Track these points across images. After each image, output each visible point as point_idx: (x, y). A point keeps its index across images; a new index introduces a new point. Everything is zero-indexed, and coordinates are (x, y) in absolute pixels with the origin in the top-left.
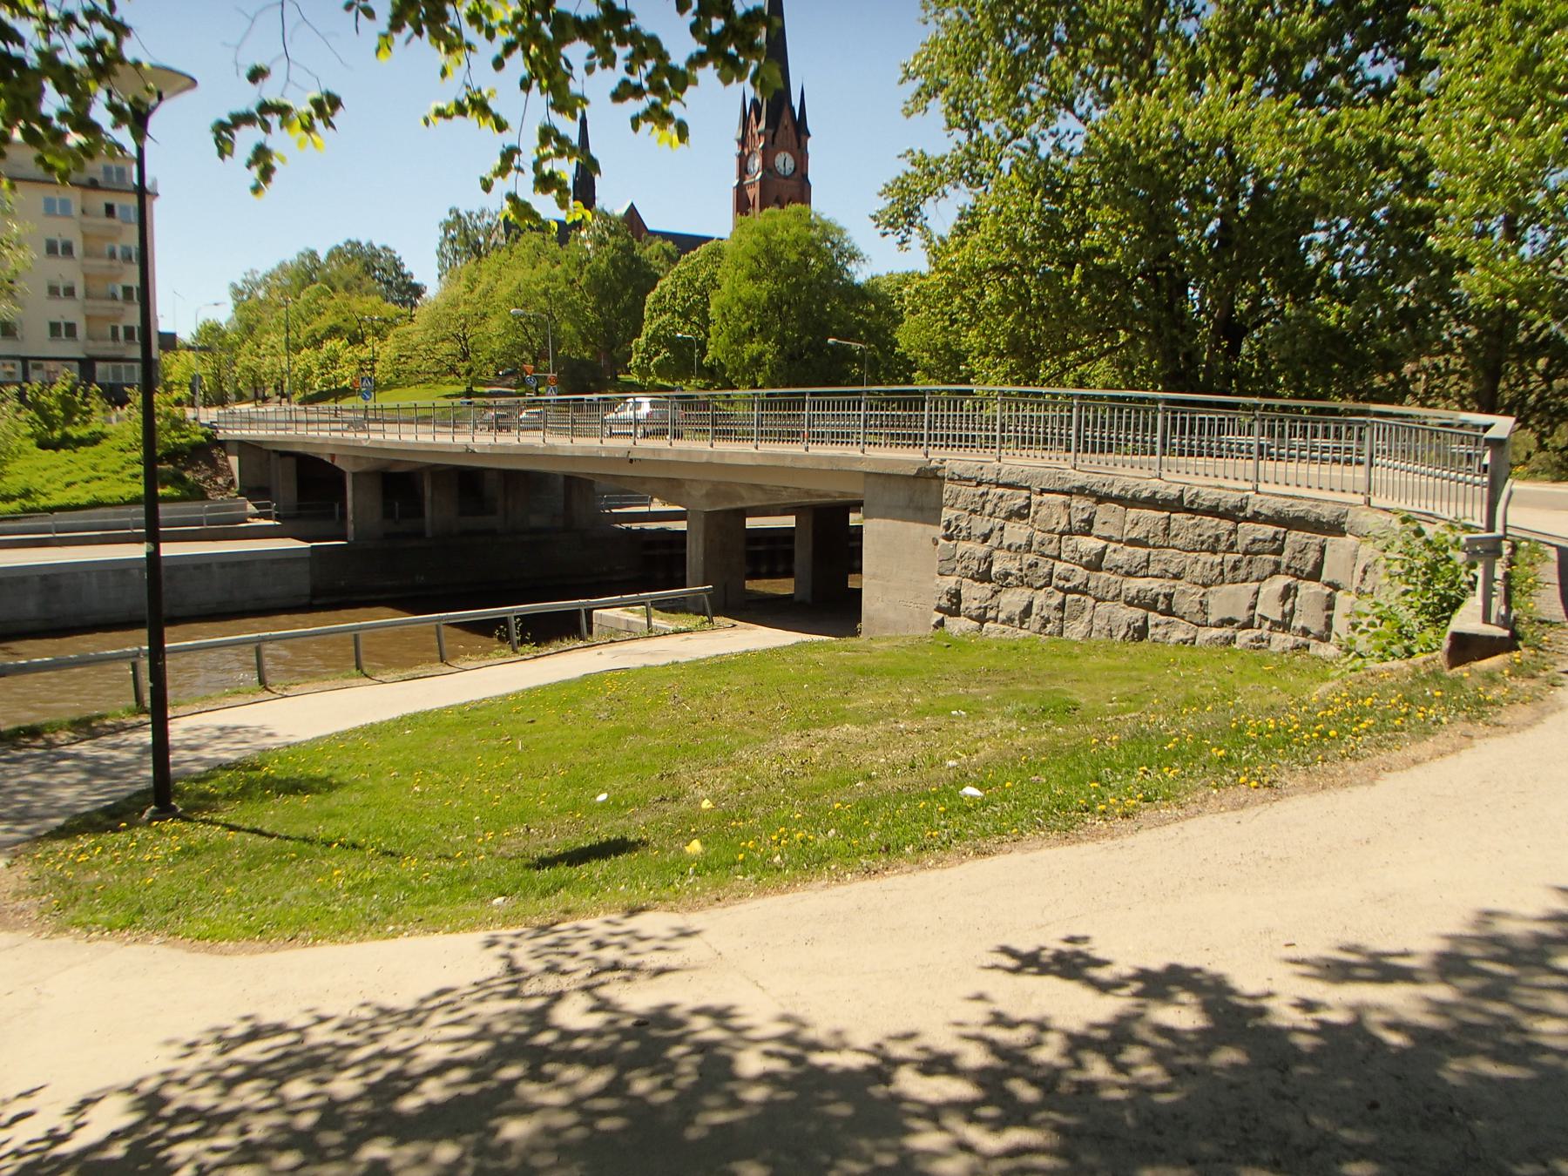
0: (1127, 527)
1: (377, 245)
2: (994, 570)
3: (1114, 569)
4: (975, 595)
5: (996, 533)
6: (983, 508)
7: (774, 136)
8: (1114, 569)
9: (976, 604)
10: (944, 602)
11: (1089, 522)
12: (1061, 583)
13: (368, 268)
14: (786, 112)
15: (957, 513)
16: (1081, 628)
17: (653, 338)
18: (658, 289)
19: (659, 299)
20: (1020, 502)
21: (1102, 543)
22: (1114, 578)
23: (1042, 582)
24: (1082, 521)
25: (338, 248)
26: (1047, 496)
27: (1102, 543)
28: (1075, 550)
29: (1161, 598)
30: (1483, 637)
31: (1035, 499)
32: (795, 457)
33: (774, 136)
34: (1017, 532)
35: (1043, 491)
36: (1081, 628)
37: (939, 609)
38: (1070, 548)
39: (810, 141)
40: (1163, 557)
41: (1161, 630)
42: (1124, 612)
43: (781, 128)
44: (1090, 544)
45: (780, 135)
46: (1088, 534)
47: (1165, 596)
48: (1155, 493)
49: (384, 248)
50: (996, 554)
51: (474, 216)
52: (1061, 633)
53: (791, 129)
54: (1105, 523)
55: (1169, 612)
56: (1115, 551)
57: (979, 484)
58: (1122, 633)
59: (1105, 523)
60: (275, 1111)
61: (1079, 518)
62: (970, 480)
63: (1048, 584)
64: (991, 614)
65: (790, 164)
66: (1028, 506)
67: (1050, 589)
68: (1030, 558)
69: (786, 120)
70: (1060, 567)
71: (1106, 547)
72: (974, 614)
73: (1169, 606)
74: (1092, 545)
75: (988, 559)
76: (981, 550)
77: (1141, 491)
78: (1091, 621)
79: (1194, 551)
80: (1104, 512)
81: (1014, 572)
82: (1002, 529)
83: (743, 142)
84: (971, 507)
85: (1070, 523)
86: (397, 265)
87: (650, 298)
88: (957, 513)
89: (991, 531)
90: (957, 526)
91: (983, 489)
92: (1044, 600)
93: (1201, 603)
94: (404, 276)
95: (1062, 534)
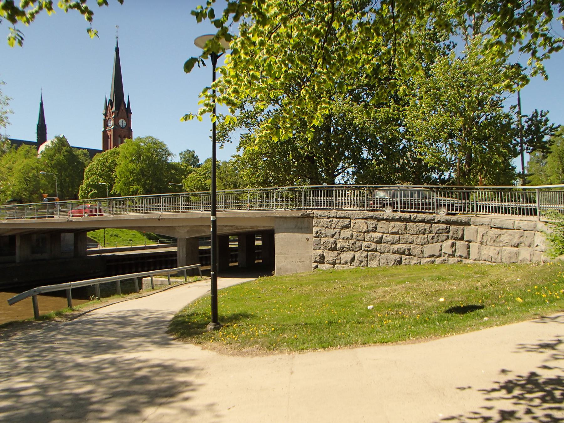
14: (122, 105)
23: (358, 249)
27: (381, 235)
33: (118, 113)
35: (356, 219)
39: (131, 115)
42: (392, 256)
43: (121, 110)
45: (120, 113)
46: (375, 231)
53: (124, 111)
62: (325, 217)
63: (361, 249)
65: (124, 123)
69: (122, 108)
71: (383, 236)
73: (410, 253)
78: (379, 260)
80: (380, 224)
82: (340, 232)
91: (330, 220)
93: (421, 251)
95: (364, 232)
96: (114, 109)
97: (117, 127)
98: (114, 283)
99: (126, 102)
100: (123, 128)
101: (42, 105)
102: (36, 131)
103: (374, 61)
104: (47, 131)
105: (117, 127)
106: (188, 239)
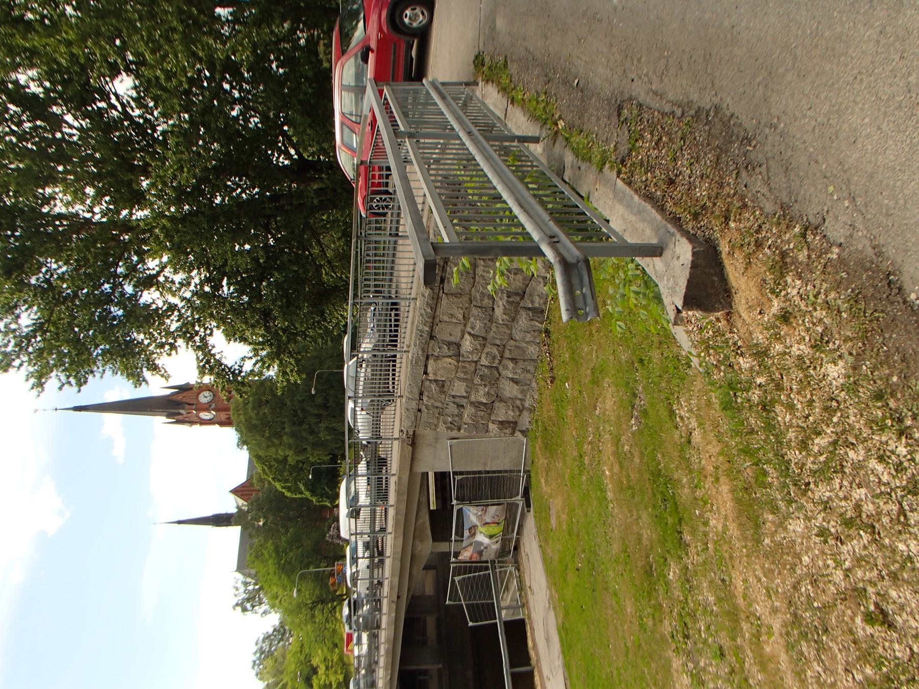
0: (455, 321)
1: (255, 648)
2: (484, 401)
3: (487, 330)
4: (502, 413)
5: (457, 400)
6: (437, 407)
7: (189, 404)
8: (487, 330)
9: (511, 413)
10: (508, 431)
11: (449, 344)
12: (497, 361)
13: (270, 654)
14: (175, 398)
15: (441, 423)
16: (532, 349)
17: (313, 492)
18: (283, 491)
19: (289, 489)
20: (433, 386)
21: (467, 336)
22: (494, 329)
23: (495, 372)
24: (449, 349)
25: (257, 675)
26: (430, 369)
27: (467, 336)
28: (472, 353)
29: (511, 299)
30: (691, 275)
31: (431, 377)
32: (397, 513)
33: (189, 404)
34: (459, 388)
35: (426, 373)
36: (532, 349)
37: (513, 434)
38: (470, 356)
40: (479, 298)
41: (537, 299)
42: (520, 322)
43: (184, 400)
44: (467, 344)
45: (188, 401)
46: (458, 346)
47: (508, 297)
48: (428, 304)
49: (257, 644)
50: (473, 398)
51: (237, 593)
52: (534, 361)
53: (185, 394)
54: (451, 335)
55: (522, 295)
56: (473, 328)
57: (419, 410)
58: (537, 324)
59: (451, 335)
60: (542, 234)
61: (447, 351)
62: (416, 417)
63: (497, 369)
64: (518, 403)
65: (207, 393)
66: (436, 381)
67: (501, 368)
68: (477, 380)
69: (180, 397)
70: (484, 361)
71: (469, 333)
72: (518, 413)
73: (517, 294)
74: (468, 343)
75: (477, 405)
76: (469, 411)
77: (426, 313)
78: (527, 343)
79: (474, 278)
80: (443, 333)
81: (487, 390)
82: (454, 397)
83: (192, 423)
84: (437, 415)
85: (450, 356)
86: (267, 637)
87: (288, 494)
88: (441, 423)
89: (454, 403)
90: (451, 423)
91: (423, 408)
92: (509, 370)
93: (515, 274)
94: (275, 630)
95: (458, 361)
96: (182, 411)
97: (213, 406)
98: (514, 676)
99: (169, 392)
100: (214, 396)
101: (180, 522)
102: (224, 528)
103: (30, 299)
104: (224, 512)
105: (213, 406)
106: (434, 540)
